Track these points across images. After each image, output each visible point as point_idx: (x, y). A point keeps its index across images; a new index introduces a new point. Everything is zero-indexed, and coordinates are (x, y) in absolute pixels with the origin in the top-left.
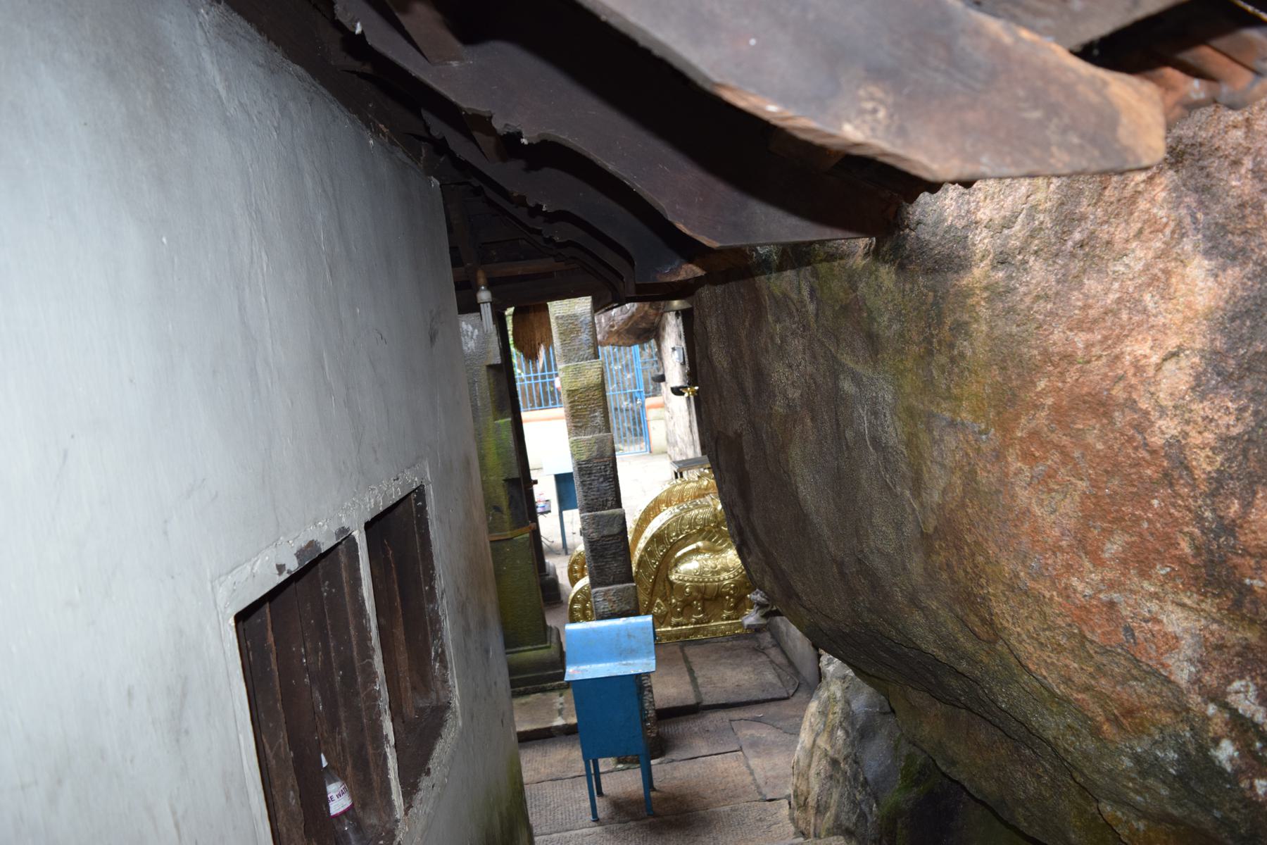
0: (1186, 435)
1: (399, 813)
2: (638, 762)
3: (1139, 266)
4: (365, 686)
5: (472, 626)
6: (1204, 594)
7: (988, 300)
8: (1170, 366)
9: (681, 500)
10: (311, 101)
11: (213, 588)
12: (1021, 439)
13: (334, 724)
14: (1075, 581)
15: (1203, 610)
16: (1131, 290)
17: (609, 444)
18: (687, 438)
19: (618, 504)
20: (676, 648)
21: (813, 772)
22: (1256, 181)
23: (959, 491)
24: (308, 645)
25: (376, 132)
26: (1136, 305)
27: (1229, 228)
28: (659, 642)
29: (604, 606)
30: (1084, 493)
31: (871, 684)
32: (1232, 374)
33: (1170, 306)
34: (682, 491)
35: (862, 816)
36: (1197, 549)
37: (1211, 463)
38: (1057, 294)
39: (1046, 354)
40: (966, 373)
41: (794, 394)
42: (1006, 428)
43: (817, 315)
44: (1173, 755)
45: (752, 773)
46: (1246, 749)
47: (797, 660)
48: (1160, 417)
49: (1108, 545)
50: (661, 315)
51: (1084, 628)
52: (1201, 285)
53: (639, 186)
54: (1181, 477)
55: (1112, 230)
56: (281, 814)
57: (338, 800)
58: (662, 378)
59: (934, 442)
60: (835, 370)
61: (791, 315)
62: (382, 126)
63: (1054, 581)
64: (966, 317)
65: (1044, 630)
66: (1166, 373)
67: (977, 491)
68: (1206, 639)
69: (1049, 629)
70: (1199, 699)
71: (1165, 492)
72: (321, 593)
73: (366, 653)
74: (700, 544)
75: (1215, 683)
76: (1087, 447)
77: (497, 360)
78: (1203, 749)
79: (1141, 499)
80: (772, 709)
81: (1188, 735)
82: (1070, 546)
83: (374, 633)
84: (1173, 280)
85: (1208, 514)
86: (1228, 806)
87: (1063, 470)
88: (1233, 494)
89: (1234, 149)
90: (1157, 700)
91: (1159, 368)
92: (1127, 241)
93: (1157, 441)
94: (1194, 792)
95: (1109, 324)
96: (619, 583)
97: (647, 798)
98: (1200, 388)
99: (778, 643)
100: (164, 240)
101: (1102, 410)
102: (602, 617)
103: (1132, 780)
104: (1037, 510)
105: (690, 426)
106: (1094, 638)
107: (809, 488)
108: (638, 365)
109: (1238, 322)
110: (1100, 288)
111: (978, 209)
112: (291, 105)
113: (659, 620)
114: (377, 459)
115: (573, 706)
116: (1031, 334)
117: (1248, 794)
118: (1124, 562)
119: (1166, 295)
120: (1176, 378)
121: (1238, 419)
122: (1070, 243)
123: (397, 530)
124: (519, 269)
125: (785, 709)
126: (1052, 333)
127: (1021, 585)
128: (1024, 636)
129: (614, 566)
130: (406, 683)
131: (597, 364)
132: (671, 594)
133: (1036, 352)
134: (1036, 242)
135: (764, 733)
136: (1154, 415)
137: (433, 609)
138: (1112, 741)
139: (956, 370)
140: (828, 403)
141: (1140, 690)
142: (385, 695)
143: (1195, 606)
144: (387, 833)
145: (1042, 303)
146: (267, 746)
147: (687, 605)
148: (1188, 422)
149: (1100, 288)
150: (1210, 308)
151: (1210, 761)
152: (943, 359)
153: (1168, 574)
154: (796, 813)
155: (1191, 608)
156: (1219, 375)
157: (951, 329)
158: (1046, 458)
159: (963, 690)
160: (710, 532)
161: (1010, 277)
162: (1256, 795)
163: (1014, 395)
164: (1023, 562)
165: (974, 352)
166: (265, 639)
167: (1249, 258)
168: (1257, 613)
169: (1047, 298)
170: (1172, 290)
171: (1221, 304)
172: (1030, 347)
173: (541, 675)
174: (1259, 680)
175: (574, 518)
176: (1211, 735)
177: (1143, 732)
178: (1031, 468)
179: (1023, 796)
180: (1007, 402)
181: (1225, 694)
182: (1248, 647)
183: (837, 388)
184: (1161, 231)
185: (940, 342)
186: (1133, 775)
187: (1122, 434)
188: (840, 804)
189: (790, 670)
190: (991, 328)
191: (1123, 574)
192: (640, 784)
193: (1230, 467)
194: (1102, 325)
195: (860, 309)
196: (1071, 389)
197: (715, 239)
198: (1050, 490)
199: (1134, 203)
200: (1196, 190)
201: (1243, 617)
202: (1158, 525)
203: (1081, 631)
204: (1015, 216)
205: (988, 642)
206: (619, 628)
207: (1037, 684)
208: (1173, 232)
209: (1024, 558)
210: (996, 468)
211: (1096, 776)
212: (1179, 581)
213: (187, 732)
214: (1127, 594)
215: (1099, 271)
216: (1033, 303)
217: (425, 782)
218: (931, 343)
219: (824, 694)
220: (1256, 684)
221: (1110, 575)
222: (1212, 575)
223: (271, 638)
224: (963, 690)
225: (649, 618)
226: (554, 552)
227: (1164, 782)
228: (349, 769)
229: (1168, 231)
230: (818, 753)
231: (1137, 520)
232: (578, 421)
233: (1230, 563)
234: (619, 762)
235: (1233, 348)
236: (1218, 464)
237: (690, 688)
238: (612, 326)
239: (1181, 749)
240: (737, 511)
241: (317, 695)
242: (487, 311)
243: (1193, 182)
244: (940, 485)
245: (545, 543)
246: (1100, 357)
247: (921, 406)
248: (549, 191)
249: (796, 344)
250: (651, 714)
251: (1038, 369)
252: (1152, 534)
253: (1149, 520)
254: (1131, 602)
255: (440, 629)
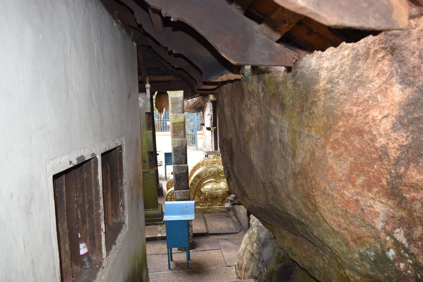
0: (388, 144)
1: (104, 256)
2: (185, 250)
3: (377, 86)
4: (96, 210)
5: (134, 197)
6: (389, 199)
7: (324, 94)
8: (384, 120)
9: (207, 165)
10: (96, 4)
11: (46, 164)
12: (332, 142)
13: (84, 223)
14: (345, 192)
15: (388, 204)
16: (373, 93)
17: (185, 142)
18: (210, 145)
19: (186, 163)
20: (201, 214)
21: (245, 257)
22: (420, 59)
23: (308, 159)
24: (77, 194)
25: (117, 22)
26: (375, 99)
27: (409, 75)
28: (196, 212)
29: (178, 197)
30: (352, 162)
31: (268, 228)
32: (405, 124)
33: (386, 100)
34: (207, 162)
35: (261, 273)
36: (388, 183)
37: (395, 154)
38: (348, 93)
39: (343, 113)
40: (315, 118)
41: (253, 125)
42: (327, 138)
43: (264, 97)
44: (373, 254)
45: (224, 257)
46: (398, 253)
47: (241, 220)
48: (380, 137)
49: (358, 180)
50: (205, 102)
51: (347, 208)
52: (397, 93)
53: (211, 40)
54: (385, 158)
55: (369, 73)
56: (62, 252)
57: (83, 250)
58: (203, 124)
59: (301, 141)
60: (268, 116)
61: (254, 97)
62: (119, 21)
63: (338, 191)
64: (316, 99)
65: (333, 208)
66: (383, 123)
67: (315, 159)
68: (388, 214)
69: (335, 208)
70: (384, 235)
71: (379, 163)
72: (83, 176)
73: (98, 199)
74: (212, 179)
75: (390, 229)
76: (354, 146)
77: (149, 111)
78: (384, 252)
79: (371, 165)
80: (232, 236)
81: (379, 247)
82: (345, 180)
83: (101, 192)
84: (388, 91)
85: (393, 171)
86: (390, 272)
87: (345, 153)
88: (402, 165)
89: (413, 48)
90: (370, 234)
91: (381, 120)
92: (374, 77)
93: (378, 145)
94: (379, 266)
95: (365, 104)
96: (184, 189)
97: (188, 263)
98: (394, 128)
99: (235, 215)
100: (40, 36)
101: (360, 133)
102: (177, 200)
103: (358, 262)
104: (335, 167)
105: (212, 141)
106: (351, 212)
107: (255, 157)
108: (196, 120)
109: (409, 107)
110: (363, 92)
111: (323, 63)
112: (89, 4)
113: (196, 204)
114: (107, 133)
115: (165, 230)
116: (338, 106)
117: (398, 268)
118: (363, 186)
119: (385, 96)
120: (386, 124)
121: (406, 140)
122: (354, 76)
123: (111, 157)
124: (160, 78)
125: (236, 236)
126: (345, 106)
127: (327, 192)
128: (326, 210)
129: (183, 184)
130: (110, 213)
131: (183, 115)
132: (201, 195)
133: (339, 112)
134: (343, 75)
135: (228, 244)
136: (378, 136)
137: (121, 189)
138: (353, 248)
139: (311, 117)
140: (265, 128)
141: (364, 231)
142: (103, 214)
143: (386, 202)
144: (99, 263)
145: (343, 96)
146: (60, 227)
147: (206, 199)
148: (389, 140)
149: (363, 92)
150: (400, 101)
151: (386, 256)
152: (307, 113)
153: (378, 191)
154: (238, 271)
155: (384, 203)
156: (401, 124)
157: (310, 103)
158: (340, 149)
159: (301, 229)
160: (216, 176)
161: (333, 87)
162: (400, 268)
163: (330, 127)
164: (328, 185)
165: (318, 112)
166: (62, 189)
167: (415, 85)
168: (407, 206)
169: (345, 94)
170: (387, 95)
171: (404, 100)
172: (337, 111)
173: (155, 219)
174: (405, 229)
175: (170, 168)
176: (387, 247)
177: (363, 245)
178: (334, 152)
179: (318, 267)
180: (328, 129)
181: (393, 233)
182: (402, 218)
183: (268, 122)
184: (385, 74)
185: (306, 108)
186: (358, 260)
187: (366, 142)
188: (253, 268)
189: (239, 224)
190: (325, 104)
191: (362, 190)
192: (186, 258)
193: (402, 156)
194: (363, 105)
195: (279, 95)
196: (350, 126)
197: (235, 60)
198: (340, 160)
199: (377, 64)
200: (398, 62)
201: (402, 207)
202: (376, 174)
203: (346, 209)
204: (336, 66)
205: (313, 212)
206: (183, 204)
207: (328, 227)
208: (389, 75)
209: (329, 183)
210: (322, 151)
211: (345, 260)
212: (381, 194)
213: (31, 213)
214: (363, 197)
215: (363, 86)
216: (340, 96)
217: (114, 247)
218: (303, 108)
219: (250, 231)
220: (404, 231)
221: (358, 190)
222: (393, 192)
223: (64, 189)
224: (301, 229)
225: (194, 202)
226: (163, 179)
227: (369, 263)
228: (88, 240)
229: (388, 75)
230: (247, 251)
231: (369, 172)
232: (175, 134)
233: (399, 188)
234: (179, 250)
235: (407, 115)
236: (398, 155)
237: (205, 227)
238: (188, 105)
239: (376, 252)
240: (228, 165)
241: (79, 212)
242: (148, 91)
243: (397, 59)
244: (302, 156)
245: (159, 176)
246: (361, 116)
247: (298, 129)
248: (177, 43)
249: (255, 107)
250: (191, 235)
251: (339, 118)
252: (373, 177)
253: (373, 172)
254: (364, 200)
255: (123, 196)
